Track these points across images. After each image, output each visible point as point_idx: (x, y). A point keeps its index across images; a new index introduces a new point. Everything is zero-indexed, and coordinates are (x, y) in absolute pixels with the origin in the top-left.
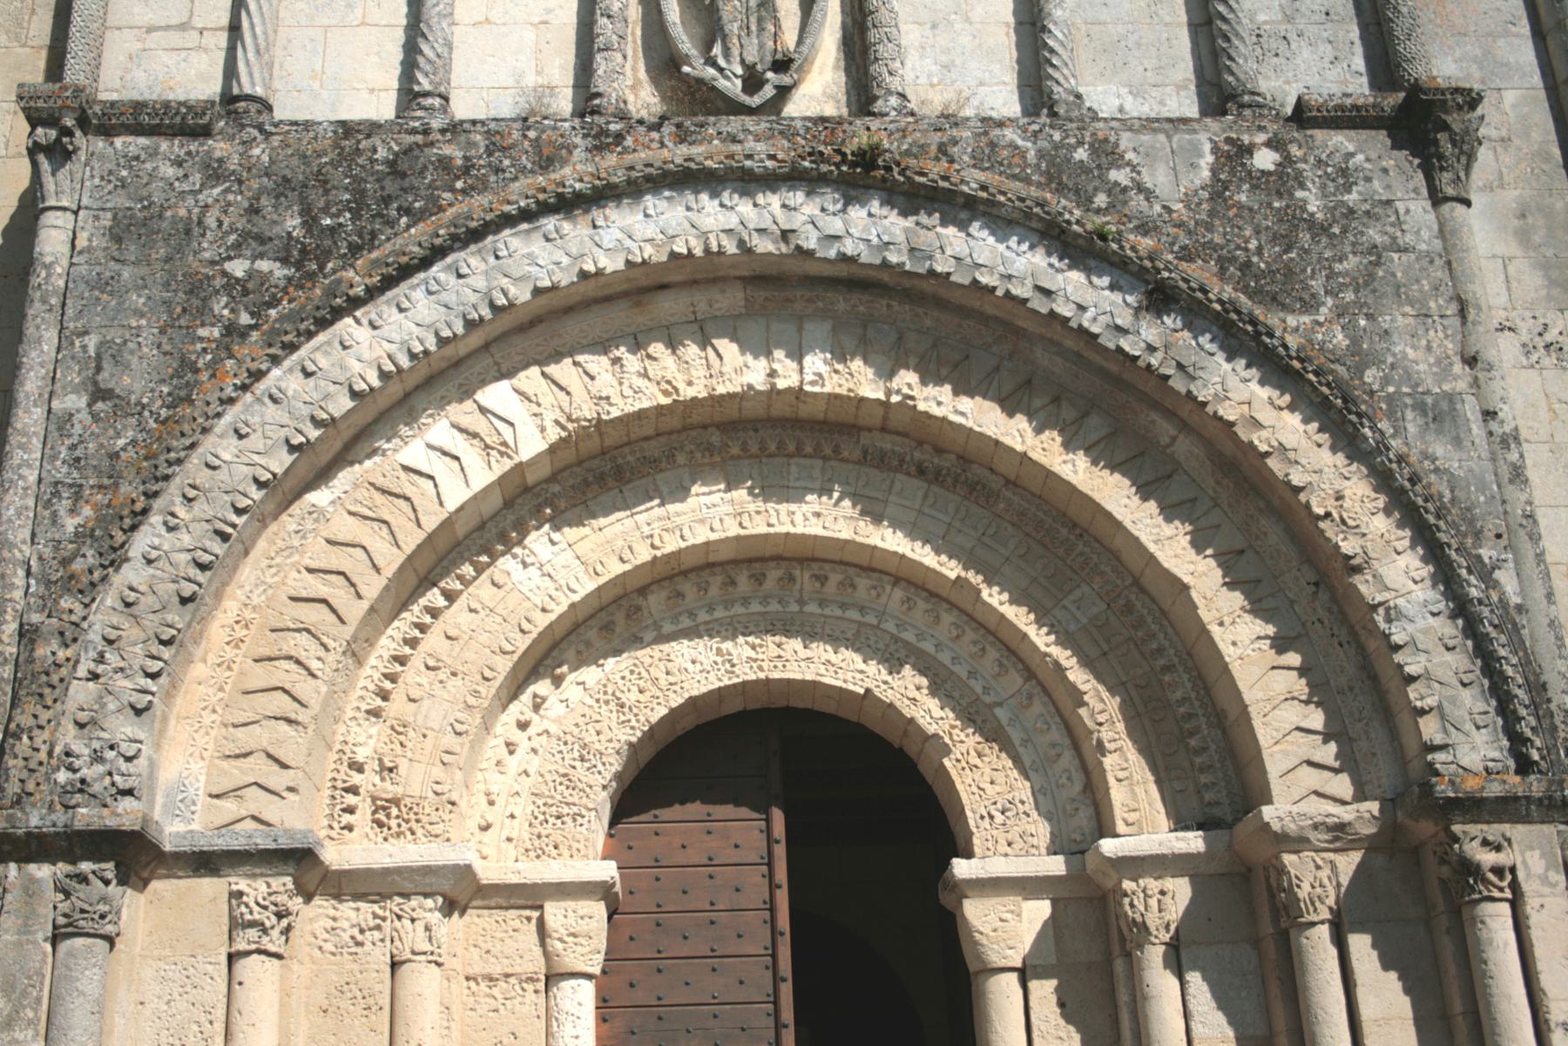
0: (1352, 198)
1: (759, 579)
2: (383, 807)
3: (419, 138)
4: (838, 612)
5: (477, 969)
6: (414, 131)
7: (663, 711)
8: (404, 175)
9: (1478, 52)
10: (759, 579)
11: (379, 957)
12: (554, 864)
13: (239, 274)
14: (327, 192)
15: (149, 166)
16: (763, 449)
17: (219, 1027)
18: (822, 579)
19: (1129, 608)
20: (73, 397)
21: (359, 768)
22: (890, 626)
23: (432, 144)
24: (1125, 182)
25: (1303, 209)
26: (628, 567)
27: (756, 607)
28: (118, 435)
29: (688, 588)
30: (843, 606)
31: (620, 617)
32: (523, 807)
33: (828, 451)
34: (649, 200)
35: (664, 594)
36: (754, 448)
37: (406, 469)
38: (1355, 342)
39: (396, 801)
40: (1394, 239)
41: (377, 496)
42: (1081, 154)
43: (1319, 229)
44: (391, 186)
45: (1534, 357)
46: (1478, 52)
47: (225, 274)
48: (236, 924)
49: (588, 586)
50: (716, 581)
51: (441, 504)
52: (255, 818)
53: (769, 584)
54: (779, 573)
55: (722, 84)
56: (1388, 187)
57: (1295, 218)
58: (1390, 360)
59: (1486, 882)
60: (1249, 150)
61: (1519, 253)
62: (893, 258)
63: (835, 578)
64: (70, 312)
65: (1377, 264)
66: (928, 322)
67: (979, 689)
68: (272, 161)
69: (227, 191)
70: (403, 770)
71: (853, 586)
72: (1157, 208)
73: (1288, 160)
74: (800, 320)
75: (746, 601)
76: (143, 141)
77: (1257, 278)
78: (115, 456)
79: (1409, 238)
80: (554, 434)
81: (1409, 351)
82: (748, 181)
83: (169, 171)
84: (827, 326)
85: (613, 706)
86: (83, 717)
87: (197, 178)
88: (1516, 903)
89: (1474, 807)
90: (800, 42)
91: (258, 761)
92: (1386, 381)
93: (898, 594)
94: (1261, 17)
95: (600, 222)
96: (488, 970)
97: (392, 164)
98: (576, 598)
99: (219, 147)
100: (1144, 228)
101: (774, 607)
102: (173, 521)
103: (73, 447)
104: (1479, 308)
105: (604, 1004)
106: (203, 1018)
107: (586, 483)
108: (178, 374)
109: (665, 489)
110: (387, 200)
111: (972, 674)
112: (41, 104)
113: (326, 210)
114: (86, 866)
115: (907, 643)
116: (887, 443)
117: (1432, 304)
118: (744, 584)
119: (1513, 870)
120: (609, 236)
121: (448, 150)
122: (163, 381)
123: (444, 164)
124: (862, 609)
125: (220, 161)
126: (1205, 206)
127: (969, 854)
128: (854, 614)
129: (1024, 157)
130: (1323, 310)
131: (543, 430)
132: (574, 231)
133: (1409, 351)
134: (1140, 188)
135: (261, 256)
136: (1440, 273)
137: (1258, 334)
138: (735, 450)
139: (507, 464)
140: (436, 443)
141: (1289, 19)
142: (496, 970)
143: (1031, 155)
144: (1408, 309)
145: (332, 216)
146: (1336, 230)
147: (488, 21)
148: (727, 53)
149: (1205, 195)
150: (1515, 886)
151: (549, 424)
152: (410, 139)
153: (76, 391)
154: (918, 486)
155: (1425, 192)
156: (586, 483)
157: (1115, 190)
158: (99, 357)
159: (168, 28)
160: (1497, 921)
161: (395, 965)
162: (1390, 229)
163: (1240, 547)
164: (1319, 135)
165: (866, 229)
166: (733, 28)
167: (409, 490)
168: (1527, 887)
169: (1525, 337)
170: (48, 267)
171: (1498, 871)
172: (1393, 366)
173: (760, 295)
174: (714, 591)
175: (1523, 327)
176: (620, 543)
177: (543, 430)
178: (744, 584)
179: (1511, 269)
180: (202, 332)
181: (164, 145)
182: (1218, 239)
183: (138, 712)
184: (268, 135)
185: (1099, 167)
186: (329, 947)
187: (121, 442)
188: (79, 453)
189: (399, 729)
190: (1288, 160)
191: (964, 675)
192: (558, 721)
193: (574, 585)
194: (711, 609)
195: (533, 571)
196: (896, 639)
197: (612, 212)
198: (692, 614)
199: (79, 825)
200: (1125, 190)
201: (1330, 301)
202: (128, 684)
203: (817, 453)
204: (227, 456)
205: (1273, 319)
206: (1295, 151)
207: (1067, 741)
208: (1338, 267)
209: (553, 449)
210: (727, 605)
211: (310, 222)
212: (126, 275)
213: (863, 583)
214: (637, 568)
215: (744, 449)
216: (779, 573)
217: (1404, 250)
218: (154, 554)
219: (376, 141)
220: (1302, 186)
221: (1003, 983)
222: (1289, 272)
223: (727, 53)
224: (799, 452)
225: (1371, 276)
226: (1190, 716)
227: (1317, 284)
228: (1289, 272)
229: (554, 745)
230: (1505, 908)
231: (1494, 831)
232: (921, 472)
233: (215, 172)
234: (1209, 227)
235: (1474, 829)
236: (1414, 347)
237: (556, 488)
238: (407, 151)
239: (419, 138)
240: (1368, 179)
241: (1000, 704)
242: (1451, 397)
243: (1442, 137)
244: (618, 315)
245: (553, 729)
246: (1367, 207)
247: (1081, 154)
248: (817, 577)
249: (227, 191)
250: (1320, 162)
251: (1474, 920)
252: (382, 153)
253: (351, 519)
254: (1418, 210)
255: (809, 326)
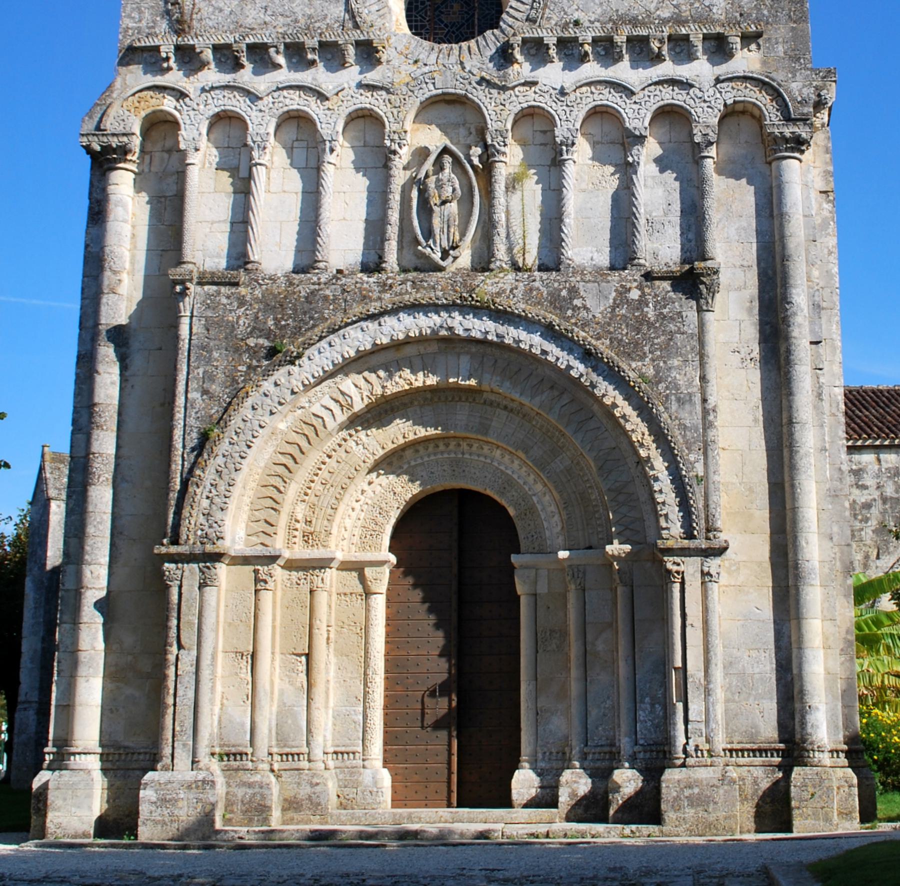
0: (665, 311)
1: (447, 445)
3: (317, 287)
4: (476, 458)
5: (341, 591)
6: (313, 284)
7: (410, 496)
8: (311, 303)
9: (746, 225)
10: (447, 445)
11: (306, 589)
12: (369, 554)
13: (252, 345)
14: (283, 309)
15: (218, 298)
16: (447, 398)
17: (253, 614)
18: (471, 446)
19: (578, 463)
20: (195, 393)
22: (496, 464)
23: (321, 290)
24: (579, 305)
25: (646, 316)
26: (395, 446)
27: (446, 456)
28: (212, 409)
29: (421, 449)
30: (479, 456)
31: (394, 459)
32: (357, 532)
33: (471, 400)
34: (401, 315)
35: (412, 451)
36: (443, 399)
37: (314, 414)
39: (312, 534)
40: (679, 328)
41: (304, 426)
42: (564, 293)
44: (306, 306)
45: (745, 364)
46: (746, 225)
47: (246, 344)
51: (325, 427)
52: (262, 544)
53: (451, 447)
54: (454, 443)
55: (433, 255)
56: (681, 306)
57: (643, 320)
58: (670, 379)
59: (674, 577)
60: (629, 290)
61: (747, 318)
63: (475, 445)
64: (192, 359)
65: (671, 339)
66: (506, 356)
67: (527, 489)
68: (263, 296)
69: (247, 309)
70: (314, 522)
71: (482, 448)
72: (590, 316)
74: (459, 355)
75: (442, 453)
76: (215, 288)
77: (624, 346)
78: (211, 416)
79: (686, 328)
81: (678, 376)
83: (224, 301)
84: (468, 357)
85: (392, 493)
86: (206, 512)
87: (235, 304)
88: (683, 584)
89: (670, 551)
90: (461, 240)
91: (262, 523)
92: (667, 388)
94: (654, 214)
95: (383, 323)
96: (345, 591)
97: (306, 298)
98: (377, 458)
99: (242, 290)
100: (584, 325)
101: (453, 455)
102: (233, 441)
103: (196, 413)
104: (708, 357)
105: (388, 601)
106: (247, 611)
109: (410, 414)
111: (524, 483)
112: (177, 277)
113: (282, 318)
114: (208, 564)
115: (502, 471)
116: (493, 397)
117: (690, 356)
118: (442, 447)
119: (683, 573)
120: (386, 329)
121: (328, 292)
122: (226, 388)
123: (326, 298)
124: (486, 457)
125: (243, 296)
126: (609, 315)
127: (518, 552)
128: (482, 459)
129: (542, 295)
130: (647, 359)
131: (362, 399)
133: (678, 376)
134: (585, 308)
135: (260, 337)
137: (619, 371)
138: (436, 399)
139: (350, 413)
140: (324, 404)
141: (666, 214)
142: (348, 591)
144: (680, 358)
145: (286, 320)
146: (657, 325)
147: (344, 219)
148: (435, 242)
149: (610, 310)
150: (683, 578)
151: (364, 397)
152: (312, 287)
153: (196, 390)
155: (695, 307)
156: (380, 414)
157: (575, 308)
158: (203, 377)
159: (220, 221)
162: (678, 324)
163: (613, 446)
164: (657, 283)
165: (480, 326)
166: (437, 231)
167: (315, 423)
169: (742, 356)
170: (183, 340)
171: (678, 572)
172: (670, 383)
174: (431, 449)
175: (742, 351)
176: (392, 436)
177: (362, 399)
178: (442, 447)
179: (742, 325)
180: (240, 368)
181: (223, 289)
182: (612, 330)
183: (222, 510)
184: (261, 285)
185: (570, 298)
186: (288, 585)
187: (213, 411)
188: (199, 415)
189: (313, 507)
190: (643, 294)
191: (522, 483)
192: (371, 498)
193: (376, 452)
194: (429, 456)
195: (361, 447)
196: (497, 468)
197: (386, 318)
198: (422, 458)
199: (207, 551)
200: (579, 308)
201: (650, 356)
202: (219, 500)
204: (250, 417)
207: (557, 511)
208: (656, 341)
209: (367, 406)
210: (435, 454)
211: (277, 321)
212: (211, 344)
213: (486, 448)
214: (399, 446)
215: (439, 399)
216: (454, 443)
217: (683, 333)
218: (226, 453)
219: (300, 287)
220: (647, 306)
223: (435, 242)
224: (460, 400)
225: (668, 344)
226: (596, 506)
227: (646, 349)
229: (371, 508)
230: (678, 585)
232: (506, 408)
233: (242, 302)
234: (609, 325)
235: (671, 559)
236: (680, 374)
237: (369, 415)
238: (312, 293)
239: (317, 287)
240: (673, 303)
241: (534, 495)
243: (702, 287)
245: (370, 502)
246: (671, 315)
247: (564, 293)
248: (468, 445)
249: (247, 309)
250: (656, 296)
251: (671, 587)
252: (303, 294)
253: (294, 434)
254: (691, 315)
255: (462, 357)
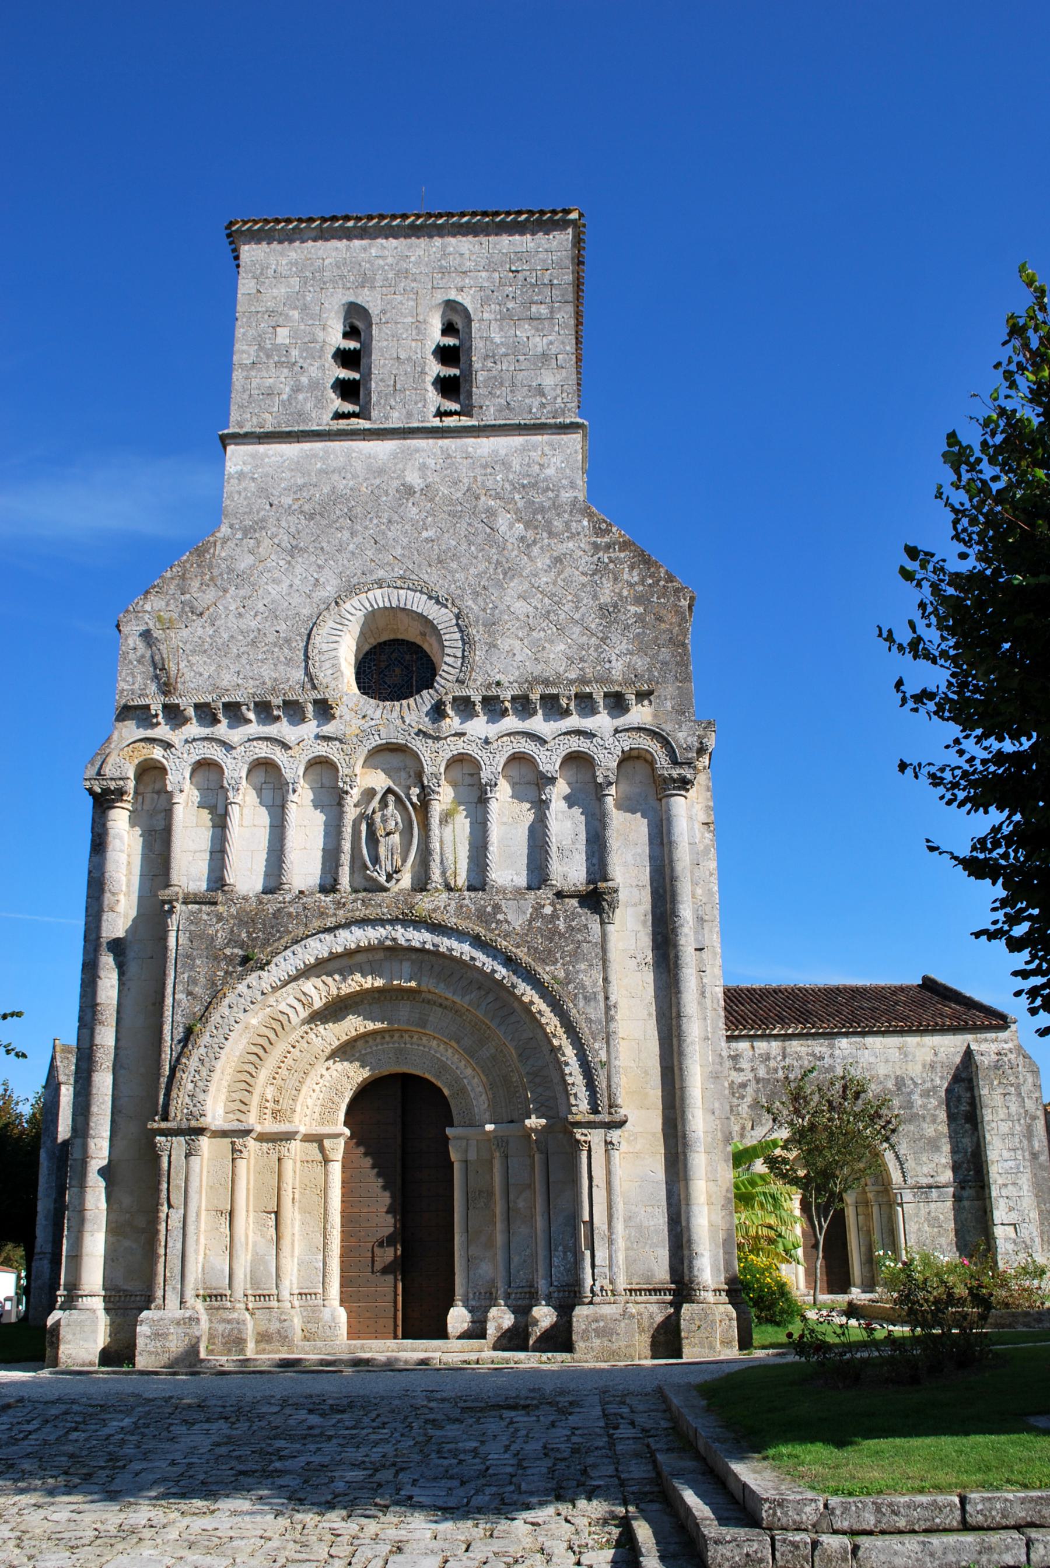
0: (574, 924)
1: (392, 1037)
2: (275, 1114)
10: (392, 1037)
18: (412, 1037)
19: (501, 1051)
21: (267, 1101)
22: (432, 1052)
30: (418, 1045)
31: (348, 1049)
32: (317, 1109)
34: (353, 928)
38: (567, 975)
42: (489, 909)
43: (561, 935)
44: (274, 921)
48: (234, 1150)
49: (337, 1043)
50: (379, 1038)
55: (379, 878)
57: (555, 932)
62: (427, 947)
63: (416, 1037)
73: (555, 909)
74: (401, 961)
75: (388, 1043)
76: (197, 906)
80: (324, 1000)
82: (381, 922)
83: (205, 917)
87: (214, 920)
88: (589, 1151)
89: (578, 1124)
92: (575, 988)
93: (435, 1042)
97: (274, 914)
99: (220, 908)
101: (397, 1045)
105: (343, 1167)
107: (336, 1011)
108: (212, 987)
110: (272, 927)
121: (291, 910)
123: (290, 914)
124: (424, 1046)
127: (452, 1126)
128: (421, 1048)
132: (328, 937)
134: (507, 921)
136: (599, 951)
139: (311, 1010)
141: (573, 843)
142: (310, 1159)
143: (473, 910)
148: (381, 867)
150: (590, 1147)
152: (279, 905)
154: (440, 1010)
156: (336, 1011)
157: (498, 922)
160: (584, 1154)
161: (279, 1160)
164: (567, 900)
167: (281, 1019)
168: (592, 1147)
171: (585, 1142)
173: (388, 954)
175: (638, 957)
180: (218, 973)
181: (204, 908)
189: (280, 1089)
190: (555, 909)
203: (408, 999)
205: (539, 970)
206: (558, 906)
213: (424, 1039)
219: (268, 906)
221: (69, 1356)
222: (550, 951)
225: (576, 951)
227: (558, 955)
228: (550, 951)
231: (585, 1131)
232: (441, 1005)
233: (220, 918)
238: (278, 910)
242: (595, 993)
244: (344, 962)
247: (489, 909)
250: (566, 911)
252: (271, 911)
254: (595, 927)
